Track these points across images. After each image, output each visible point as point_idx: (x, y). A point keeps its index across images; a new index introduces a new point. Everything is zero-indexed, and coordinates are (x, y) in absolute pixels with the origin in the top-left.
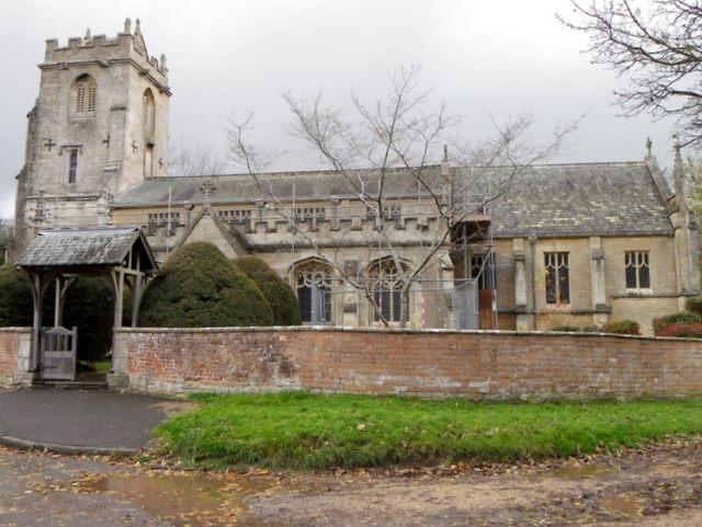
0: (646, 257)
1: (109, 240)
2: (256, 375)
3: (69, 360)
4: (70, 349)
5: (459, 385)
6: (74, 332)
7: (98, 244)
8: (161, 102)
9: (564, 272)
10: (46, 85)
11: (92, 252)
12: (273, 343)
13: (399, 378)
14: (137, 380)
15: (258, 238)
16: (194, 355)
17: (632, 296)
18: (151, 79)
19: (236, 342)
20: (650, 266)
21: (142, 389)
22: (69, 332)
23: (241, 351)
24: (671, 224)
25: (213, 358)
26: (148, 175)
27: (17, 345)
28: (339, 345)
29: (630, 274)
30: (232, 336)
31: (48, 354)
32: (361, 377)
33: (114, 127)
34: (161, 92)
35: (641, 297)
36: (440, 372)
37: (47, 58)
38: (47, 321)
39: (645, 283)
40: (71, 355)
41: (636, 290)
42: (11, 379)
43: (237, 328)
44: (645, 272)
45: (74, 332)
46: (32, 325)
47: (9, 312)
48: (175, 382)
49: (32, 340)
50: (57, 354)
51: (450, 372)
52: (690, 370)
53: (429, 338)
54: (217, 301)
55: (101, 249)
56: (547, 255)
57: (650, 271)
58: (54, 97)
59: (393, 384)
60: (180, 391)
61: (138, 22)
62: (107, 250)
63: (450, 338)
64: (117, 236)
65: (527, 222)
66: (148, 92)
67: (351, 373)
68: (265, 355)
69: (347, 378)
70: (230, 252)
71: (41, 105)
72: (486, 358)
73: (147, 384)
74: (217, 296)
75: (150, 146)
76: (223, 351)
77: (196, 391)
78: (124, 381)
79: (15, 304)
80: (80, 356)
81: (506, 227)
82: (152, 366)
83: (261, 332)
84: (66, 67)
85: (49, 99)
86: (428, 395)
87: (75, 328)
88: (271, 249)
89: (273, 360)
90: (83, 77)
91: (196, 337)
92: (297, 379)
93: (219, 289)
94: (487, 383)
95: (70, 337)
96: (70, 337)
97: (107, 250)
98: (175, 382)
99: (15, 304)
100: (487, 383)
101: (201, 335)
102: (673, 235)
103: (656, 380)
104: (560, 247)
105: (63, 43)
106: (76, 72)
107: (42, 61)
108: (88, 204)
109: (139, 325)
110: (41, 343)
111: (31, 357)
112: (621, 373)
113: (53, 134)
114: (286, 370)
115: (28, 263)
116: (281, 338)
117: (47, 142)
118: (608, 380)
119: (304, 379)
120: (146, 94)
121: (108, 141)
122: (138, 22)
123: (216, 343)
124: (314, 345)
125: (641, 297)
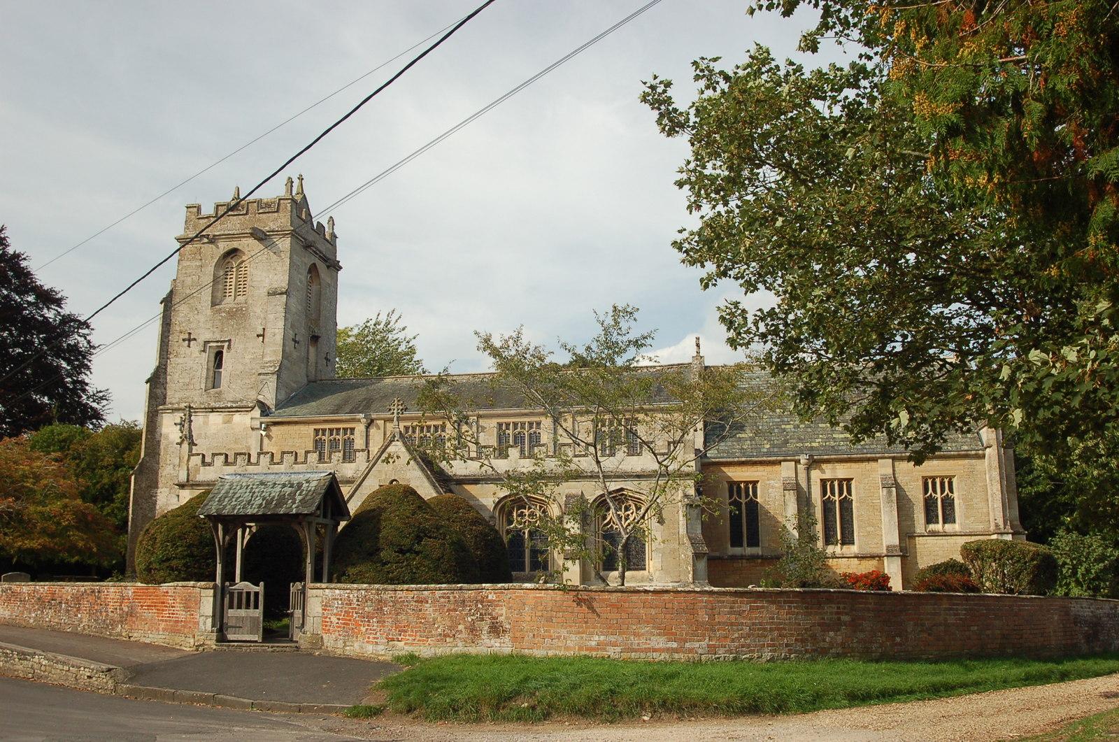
0: (950, 484)
1: (300, 485)
2: (464, 635)
3: (254, 619)
4: (256, 607)
5: (675, 645)
6: (260, 588)
7: (288, 490)
8: (328, 280)
9: (846, 506)
10: (185, 263)
11: (282, 500)
12: (482, 602)
13: (612, 638)
14: (333, 643)
15: (458, 468)
16: (397, 614)
17: (934, 534)
18: (317, 253)
19: (442, 600)
20: (955, 495)
21: (339, 652)
22: (256, 589)
23: (449, 610)
24: (981, 440)
25: (418, 618)
26: (312, 377)
27: (198, 602)
28: (550, 604)
29: (929, 505)
30: (438, 594)
31: (231, 613)
32: (573, 637)
33: (271, 317)
34: (328, 267)
35: (946, 535)
36: (656, 631)
37: (187, 228)
38: (229, 576)
39: (949, 518)
40: (258, 613)
41: (938, 527)
42: (192, 641)
43: (444, 586)
44: (948, 504)
45: (260, 588)
46: (214, 580)
47: (184, 565)
48: (377, 643)
49: (215, 596)
50: (242, 612)
51: (667, 632)
52: (942, 628)
53: (643, 597)
54: (417, 553)
55: (292, 495)
56: (823, 482)
57: (956, 502)
58: (195, 278)
59: (607, 645)
60: (383, 652)
61: (301, 178)
62: (298, 498)
63: (666, 597)
64: (308, 481)
65: (800, 440)
66: (313, 269)
67: (563, 632)
68: (473, 615)
69: (559, 638)
70: (427, 491)
71: (179, 288)
72: (704, 617)
73: (345, 646)
74: (417, 548)
75: (315, 339)
76: (429, 609)
77: (400, 653)
78: (318, 641)
79: (191, 555)
80: (268, 615)
81: (773, 446)
82: (349, 630)
83: (470, 591)
84: (213, 240)
85: (189, 281)
86: (643, 655)
87: (262, 584)
88: (475, 481)
89: (482, 620)
90: (233, 253)
91: (399, 594)
92: (507, 639)
93: (419, 539)
94: (704, 644)
95: (257, 594)
96: (257, 594)
97: (298, 498)
98: (377, 643)
99: (191, 555)
100: (704, 644)
101: (405, 593)
102: (984, 456)
103: (898, 639)
104: (841, 471)
105: (208, 210)
106: (224, 246)
107: (180, 232)
108: (237, 418)
109: (330, 581)
110: (224, 600)
111: (214, 616)
112: (855, 632)
113: (193, 326)
114: (496, 630)
115: (213, 512)
116: (490, 597)
117: (186, 336)
118: (839, 639)
119: (514, 639)
120: (310, 271)
121: (263, 336)
122: (301, 178)
123: (422, 602)
124: (524, 604)
125: (946, 535)
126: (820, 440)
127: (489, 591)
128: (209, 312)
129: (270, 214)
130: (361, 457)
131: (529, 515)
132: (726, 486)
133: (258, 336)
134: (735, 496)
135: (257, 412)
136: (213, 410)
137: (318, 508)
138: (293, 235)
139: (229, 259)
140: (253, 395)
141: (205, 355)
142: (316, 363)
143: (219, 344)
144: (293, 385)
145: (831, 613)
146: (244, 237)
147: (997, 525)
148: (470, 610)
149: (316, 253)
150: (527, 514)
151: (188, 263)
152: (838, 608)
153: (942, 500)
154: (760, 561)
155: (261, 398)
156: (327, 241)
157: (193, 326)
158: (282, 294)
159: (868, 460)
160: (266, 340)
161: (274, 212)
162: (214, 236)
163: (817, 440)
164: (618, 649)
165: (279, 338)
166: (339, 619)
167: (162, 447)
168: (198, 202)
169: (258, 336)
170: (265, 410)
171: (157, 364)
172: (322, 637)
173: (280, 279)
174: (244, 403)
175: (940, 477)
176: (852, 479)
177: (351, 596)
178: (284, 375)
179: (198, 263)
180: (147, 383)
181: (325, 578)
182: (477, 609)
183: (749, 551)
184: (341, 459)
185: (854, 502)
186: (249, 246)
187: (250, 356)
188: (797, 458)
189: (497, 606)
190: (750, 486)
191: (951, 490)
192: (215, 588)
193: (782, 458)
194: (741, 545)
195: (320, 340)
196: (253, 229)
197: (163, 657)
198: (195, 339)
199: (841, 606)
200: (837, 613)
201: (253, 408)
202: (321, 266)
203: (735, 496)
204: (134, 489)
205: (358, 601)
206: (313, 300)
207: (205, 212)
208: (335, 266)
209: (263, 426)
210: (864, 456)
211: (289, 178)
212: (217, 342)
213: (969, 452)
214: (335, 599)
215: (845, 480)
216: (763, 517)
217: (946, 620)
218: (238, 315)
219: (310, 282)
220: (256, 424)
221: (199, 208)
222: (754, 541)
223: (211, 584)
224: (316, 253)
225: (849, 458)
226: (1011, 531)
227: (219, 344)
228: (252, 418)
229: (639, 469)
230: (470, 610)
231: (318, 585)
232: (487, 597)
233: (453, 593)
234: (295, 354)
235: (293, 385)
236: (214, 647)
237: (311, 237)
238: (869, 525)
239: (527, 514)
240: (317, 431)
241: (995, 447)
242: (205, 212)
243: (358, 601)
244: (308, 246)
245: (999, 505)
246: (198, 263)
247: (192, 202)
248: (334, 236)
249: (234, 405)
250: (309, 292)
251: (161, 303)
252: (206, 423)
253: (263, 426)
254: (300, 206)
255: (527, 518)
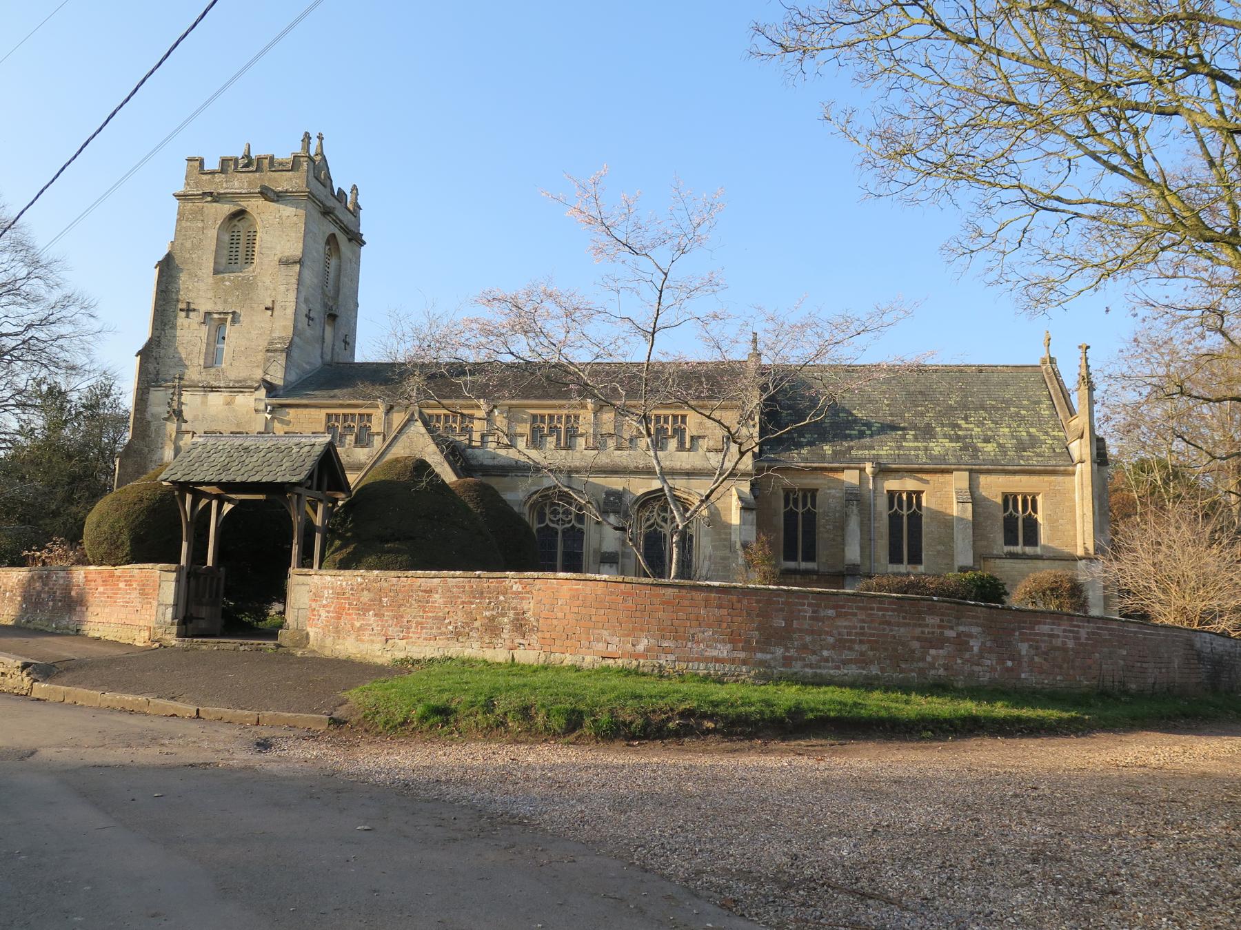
0: (1034, 502)
18: (337, 222)
21: (327, 653)
30: (451, 582)
34: (350, 240)
37: (188, 184)
46: (179, 562)
66: (332, 240)
75: (332, 317)
84: (217, 198)
90: (240, 214)
103: (1009, 664)
105: (212, 164)
107: (181, 189)
108: (240, 399)
120: (328, 242)
126: (888, 448)
127: (513, 580)
128: (211, 280)
129: (284, 173)
130: (377, 440)
131: (563, 513)
132: (782, 493)
133: (266, 309)
134: (791, 505)
135: (262, 393)
136: (213, 389)
137: (310, 477)
138: (309, 198)
139: (235, 222)
140: (258, 374)
141: (205, 328)
142: (334, 345)
143: (222, 316)
144: (305, 365)
145: (933, 626)
146: (254, 197)
147: (1086, 549)
148: (490, 603)
149: (337, 223)
150: (561, 512)
151: (188, 224)
152: (942, 621)
153: (1024, 520)
154: (815, 577)
155: (268, 378)
156: (349, 210)
157: (191, 294)
158: (295, 262)
159: (943, 471)
160: (276, 313)
161: (289, 171)
162: (219, 194)
163: (884, 448)
164: (671, 657)
165: (290, 311)
166: (328, 612)
167: (153, 428)
168: (203, 156)
169: (266, 309)
170: (271, 389)
171: (150, 336)
172: (308, 634)
173: (294, 248)
174: (249, 383)
175: (1022, 493)
176: (923, 492)
177: (344, 583)
178: (295, 353)
179: (200, 225)
180: (137, 356)
181: (316, 566)
182: (498, 603)
183: (804, 565)
184: (353, 443)
185: (923, 518)
186: (255, 206)
187: (257, 332)
188: (862, 465)
189: (523, 598)
190: (809, 495)
191: (1035, 509)
192: (179, 571)
193: (846, 465)
194: (795, 559)
195: (338, 319)
196: (263, 187)
197: (117, 652)
198: (194, 310)
199: (945, 618)
200: (940, 627)
201: (257, 389)
202: (341, 238)
203: (791, 505)
204: (118, 474)
205: (352, 589)
206: (332, 275)
207: (207, 167)
208: (356, 239)
209: (269, 408)
210: (938, 466)
211: (306, 133)
212: (220, 313)
213: (1057, 468)
214: (325, 588)
215: (915, 492)
216: (822, 529)
217: (1064, 643)
218: (247, 288)
219: (328, 256)
220: (262, 407)
221: (202, 162)
222: (810, 556)
223: (173, 566)
224: (337, 223)
225: (921, 469)
226: (713, 664)
227: (222, 316)
228: (256, 400)
229: (689, 467)
230: (490, 603)
231: (305, 570)
232: (512, 587)
233: (469, 582)
234: (309, 332)
235: (305, 365)
236: (174, 642)
237: (332, 203)
238: (940, 544)
239: (561, 512)
240: (329, 415)
241: (1088, 463)
242: (207, 167)
243: (352, 589)
244: (327, 212)
245: (1089, 527)
246: (200, 225)
247: (196, 155)
248: (357, 207)
249: (237, 385)
250: (327, 265)
251: (156, 267)
252: (204, 403)
253: (269, 408)
254: (318, 169)
255: (561, 516)
